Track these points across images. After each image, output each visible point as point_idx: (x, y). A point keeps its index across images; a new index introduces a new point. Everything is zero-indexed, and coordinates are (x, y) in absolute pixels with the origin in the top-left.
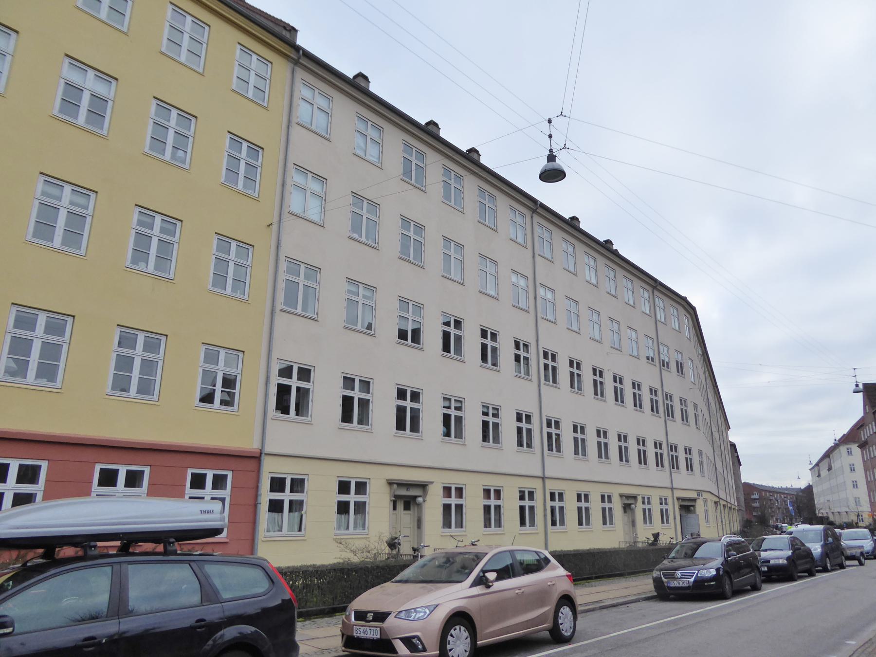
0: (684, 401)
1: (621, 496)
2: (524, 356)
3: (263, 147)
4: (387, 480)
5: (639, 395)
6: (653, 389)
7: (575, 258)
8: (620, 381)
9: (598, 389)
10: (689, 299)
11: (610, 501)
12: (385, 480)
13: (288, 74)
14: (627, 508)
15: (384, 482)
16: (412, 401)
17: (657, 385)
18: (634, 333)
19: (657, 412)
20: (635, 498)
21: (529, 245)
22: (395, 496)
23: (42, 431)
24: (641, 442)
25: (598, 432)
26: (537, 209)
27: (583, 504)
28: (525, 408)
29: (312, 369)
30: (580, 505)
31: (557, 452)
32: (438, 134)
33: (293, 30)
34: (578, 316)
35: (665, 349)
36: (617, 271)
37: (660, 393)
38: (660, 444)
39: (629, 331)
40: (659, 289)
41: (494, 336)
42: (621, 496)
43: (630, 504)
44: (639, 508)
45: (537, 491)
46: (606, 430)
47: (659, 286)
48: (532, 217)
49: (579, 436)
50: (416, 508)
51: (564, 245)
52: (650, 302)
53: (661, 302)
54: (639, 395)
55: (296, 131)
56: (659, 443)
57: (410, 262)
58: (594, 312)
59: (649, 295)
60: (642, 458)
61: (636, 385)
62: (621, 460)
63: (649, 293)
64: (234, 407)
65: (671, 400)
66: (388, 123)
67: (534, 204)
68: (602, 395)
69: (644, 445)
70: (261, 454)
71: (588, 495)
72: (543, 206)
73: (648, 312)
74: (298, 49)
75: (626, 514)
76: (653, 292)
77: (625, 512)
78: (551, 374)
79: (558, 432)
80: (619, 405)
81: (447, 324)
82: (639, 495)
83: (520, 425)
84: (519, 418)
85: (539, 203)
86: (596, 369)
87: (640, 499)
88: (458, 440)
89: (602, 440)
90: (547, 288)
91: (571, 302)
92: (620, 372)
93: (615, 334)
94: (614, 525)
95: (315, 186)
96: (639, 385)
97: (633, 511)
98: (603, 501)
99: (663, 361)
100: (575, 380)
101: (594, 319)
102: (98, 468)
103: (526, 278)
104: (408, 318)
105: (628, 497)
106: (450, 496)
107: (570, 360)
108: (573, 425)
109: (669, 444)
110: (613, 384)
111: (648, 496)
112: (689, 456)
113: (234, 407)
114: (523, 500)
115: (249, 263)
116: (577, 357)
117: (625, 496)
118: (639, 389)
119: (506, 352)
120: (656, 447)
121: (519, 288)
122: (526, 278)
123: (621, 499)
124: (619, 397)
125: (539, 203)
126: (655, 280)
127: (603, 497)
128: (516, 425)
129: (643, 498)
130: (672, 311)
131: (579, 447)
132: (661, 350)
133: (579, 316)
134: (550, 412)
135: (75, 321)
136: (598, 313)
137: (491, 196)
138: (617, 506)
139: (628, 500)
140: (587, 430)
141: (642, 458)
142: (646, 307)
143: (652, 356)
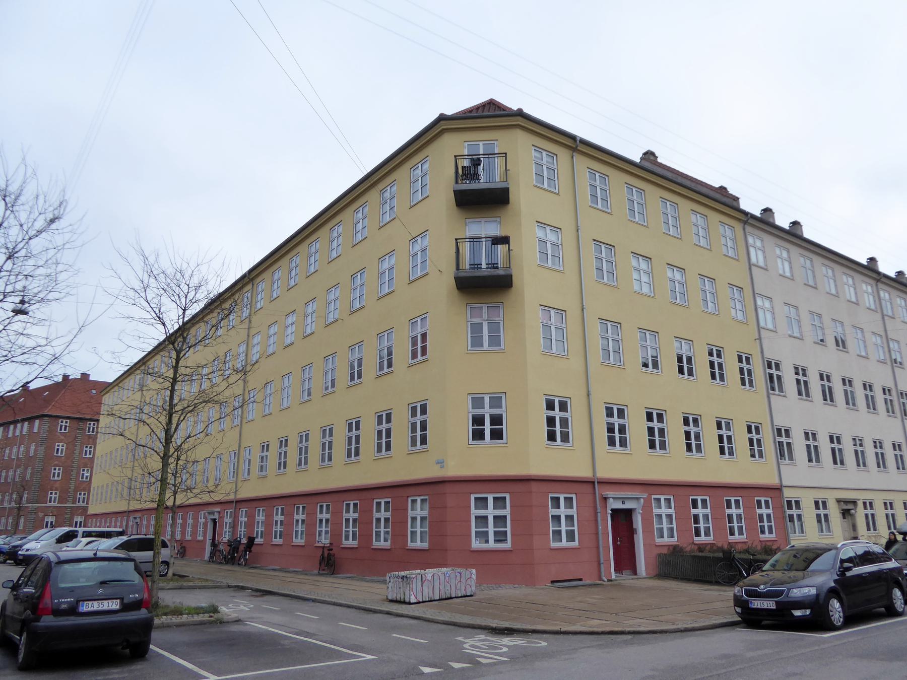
0: (802, 369)
1: (839, 501)
2: (804, 380)
3: (684, 268)
4: (836, 499)
5: (851, 392)
6: (847, 379)
7: (813, 272)
8: (776, 366)
9: (828, 395)
10: (527, 110)
11: (825, 507)
12: (835, 499)
13: (570, 158)
14: (846, 513)
15: (834, 500)
16: (619, 417)
17: (890, 384)
18: (793, 310)
19: (893, 413)
20: (854, 502)
21: (879, 310)
22: (843, 510)
23: (459, 474)
24: (877, 444)
25: (831, 438)
26: (748, 219)
27: (890, 512)
28: (754, 419)
29: (625, 408)
30: (818, 512)
31: (759, 458)
32: (800, 234)
33: (736, 199)
34: (799, 321)
35: (896, 345)
36: (790, 250)
37: (894, 392)
38: (899, 446)
39: (786, 308)
40: (751, 222)
41: (778, 366)
42: (839, 501)
43: (849, 510)
44: (860, 514)
45: (829, 501)
46: (839, 436)
47: (751, 219)
48: (744, 229)
49: (812, 443)
50: (850, 517)
51: (802, 259)
52: (874, 297)
53: (887, 295)
54: (851, 392)
55: (753, 268)
56: (785, 430)
57: (549, 269)
58: (815, 316)
59: (872, 290)
60: (881, 461)
61: (868, 387)
62: (835, 462)
63: (872, 287)
64: (503, 439)
65: (871, 390)
66: (614, 170)
67: (877, 275)
68: (832, 400)
69: (881, 447)
70: (781, 486)
71: (825, 501)
72: (584, 142)
73: (873, 307)
74: (879, 273)
75: (845, 520)
76: (877, 285)
77: (844, 518)
78: (774, 382)
79: (788, 440)
80: (828, 405)
81: (770, 367)
82: (859, 500)
83: (651, 424)
84: (686, 422)
85: (578, 139)
86: (771, 362)
87: (860, 504)
88: (623, 449)
89: (836, 446)
90: (764, 298)
91: (791, 309)
92: (826, 369)
93: (860, 341)
94: (805, 534)
95: (643, 265)
96: (850, 381)
97: (852, 516)
98: (817, 507)
99: (895, 360)
100: (803, 389)
101: (792, 314)
102: (473, 497)
103: (880, 336)
104: (608, 339)
105: (847, 502)
106: (558, 507)
107: (795, 367)
108: (830, 435)
109: (775, 427)
110: (863, 392)
111: (870, 501)
112: (879, 451)
113: (503, 439)
114: (696, 509)
115: (657, 346)
116: (848, 375)
117: (843, 501)
118: (851, 385)
119: (732, 368)
120: (895, 449)
121: (765, 310)
122: (880, 336)
123: (839, 505)
124: (850, 400)
125: (578, 139)
126: (573, 137)
127: (817, 503)
128: (545, 413)
129: (865, 503)
130: (825, 272)
131: (813, 455)
132: (891, 346)
133: (774, 313)
134: (781, 421)
135: (629, 409)
136: (796, 308)
137: (641, 191)
138: (834, 512)
139: (846, 505)
140: (843, 440)
141: (881, 461)
142: (869, 300)
143: (900, 361)
